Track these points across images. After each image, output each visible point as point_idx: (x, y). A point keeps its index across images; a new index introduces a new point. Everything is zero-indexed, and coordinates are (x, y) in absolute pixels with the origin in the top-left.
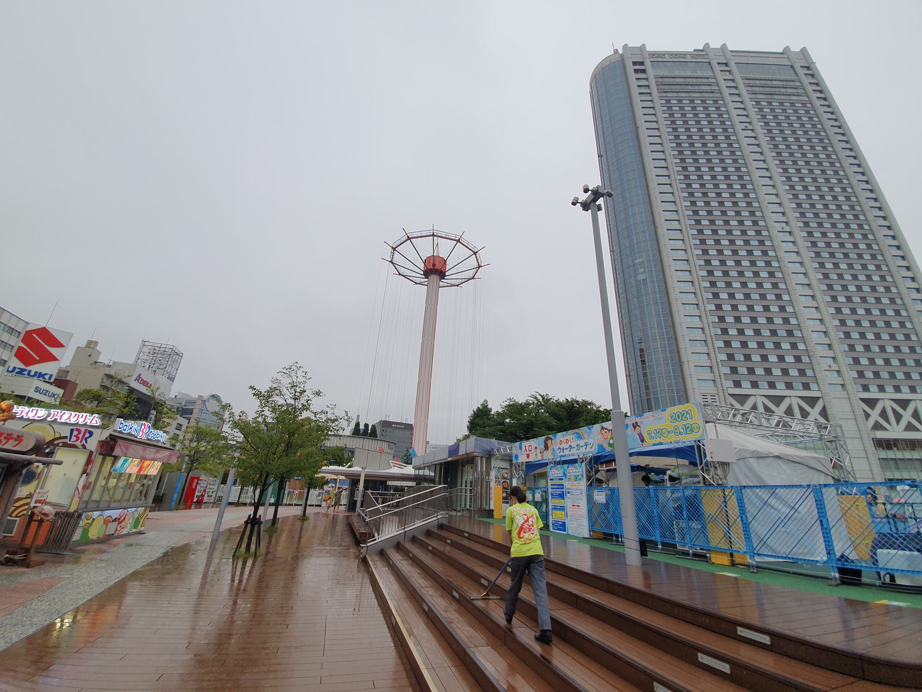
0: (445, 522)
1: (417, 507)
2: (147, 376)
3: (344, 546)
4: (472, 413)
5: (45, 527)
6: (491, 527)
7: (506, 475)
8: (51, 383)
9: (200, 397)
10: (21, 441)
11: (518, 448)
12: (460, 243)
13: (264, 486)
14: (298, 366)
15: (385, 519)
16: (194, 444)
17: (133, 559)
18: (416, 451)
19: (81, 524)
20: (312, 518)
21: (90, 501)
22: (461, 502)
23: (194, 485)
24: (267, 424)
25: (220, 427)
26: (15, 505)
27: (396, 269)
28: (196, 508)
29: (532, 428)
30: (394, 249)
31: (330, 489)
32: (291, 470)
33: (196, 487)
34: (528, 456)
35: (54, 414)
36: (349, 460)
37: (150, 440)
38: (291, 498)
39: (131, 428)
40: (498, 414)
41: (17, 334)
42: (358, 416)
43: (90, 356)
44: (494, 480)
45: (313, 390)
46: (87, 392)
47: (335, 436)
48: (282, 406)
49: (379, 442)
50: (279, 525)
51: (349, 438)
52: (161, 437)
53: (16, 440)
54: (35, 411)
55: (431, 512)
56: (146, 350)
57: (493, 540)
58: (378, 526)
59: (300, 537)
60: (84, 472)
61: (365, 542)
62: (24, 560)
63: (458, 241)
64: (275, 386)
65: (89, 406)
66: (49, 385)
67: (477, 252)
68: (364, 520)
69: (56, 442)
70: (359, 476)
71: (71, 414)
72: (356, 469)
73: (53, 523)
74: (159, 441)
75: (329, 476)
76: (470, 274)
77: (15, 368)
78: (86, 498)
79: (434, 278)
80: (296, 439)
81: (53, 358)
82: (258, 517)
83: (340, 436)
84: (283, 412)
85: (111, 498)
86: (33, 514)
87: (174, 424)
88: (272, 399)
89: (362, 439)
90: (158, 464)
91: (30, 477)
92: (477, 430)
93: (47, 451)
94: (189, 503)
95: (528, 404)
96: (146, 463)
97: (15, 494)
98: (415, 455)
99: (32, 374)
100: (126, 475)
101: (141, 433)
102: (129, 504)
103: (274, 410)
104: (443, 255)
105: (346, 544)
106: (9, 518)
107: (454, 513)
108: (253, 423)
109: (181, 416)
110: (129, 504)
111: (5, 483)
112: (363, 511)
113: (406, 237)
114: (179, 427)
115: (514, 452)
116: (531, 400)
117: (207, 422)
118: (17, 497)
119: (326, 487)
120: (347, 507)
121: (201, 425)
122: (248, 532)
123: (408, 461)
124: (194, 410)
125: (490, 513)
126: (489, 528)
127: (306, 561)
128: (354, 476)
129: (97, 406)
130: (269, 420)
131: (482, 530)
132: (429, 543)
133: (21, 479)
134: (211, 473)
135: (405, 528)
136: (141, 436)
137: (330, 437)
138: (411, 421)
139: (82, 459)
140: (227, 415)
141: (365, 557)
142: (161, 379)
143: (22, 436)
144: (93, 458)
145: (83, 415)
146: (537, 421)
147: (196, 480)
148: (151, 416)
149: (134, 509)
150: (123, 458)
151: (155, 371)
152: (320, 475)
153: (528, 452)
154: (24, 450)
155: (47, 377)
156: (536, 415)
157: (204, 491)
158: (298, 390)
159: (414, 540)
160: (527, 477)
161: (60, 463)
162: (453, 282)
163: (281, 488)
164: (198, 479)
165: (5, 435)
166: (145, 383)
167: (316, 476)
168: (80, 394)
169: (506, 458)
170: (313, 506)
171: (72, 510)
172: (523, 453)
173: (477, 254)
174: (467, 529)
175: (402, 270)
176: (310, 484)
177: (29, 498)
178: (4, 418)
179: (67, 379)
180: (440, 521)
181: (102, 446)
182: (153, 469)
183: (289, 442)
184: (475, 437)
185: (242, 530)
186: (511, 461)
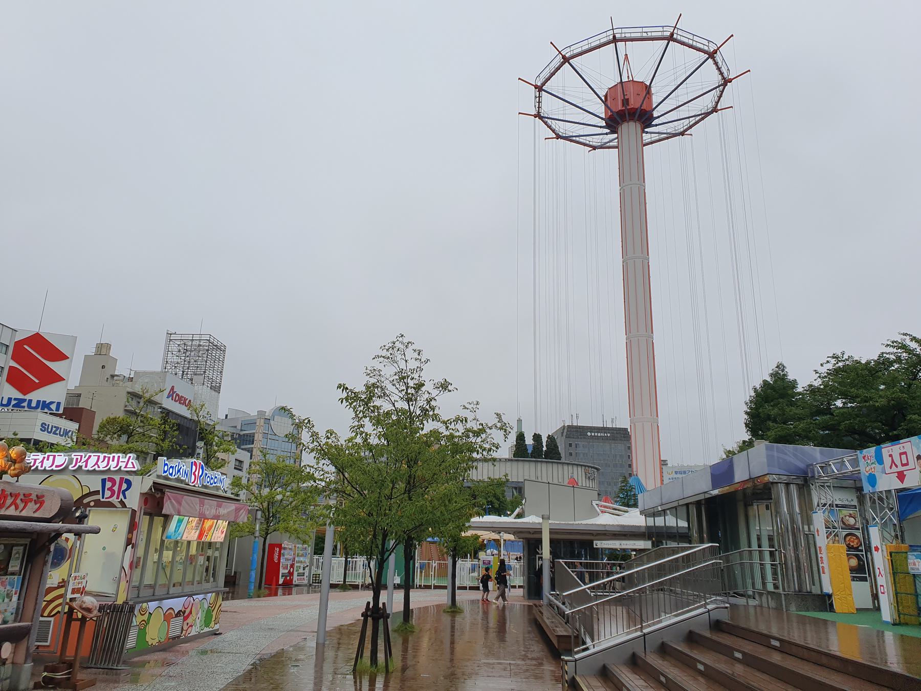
0: (725, 617)
1: (660, 588)
2: (183, 389)
3: (532, 659)
4: (753, 394)
5: (90, 627)
6: (831, 629)
7: (852, 521)
8: (60, 416)
9: (261, 413)
10: (42, 503)
11: (873, 460)
12: (676, 41)
13: (382, 553)
14: (405, 340)
15: (601, 612)
16: (266, 491)
17: (213, 673)
18: (643, 481)
19: (136, 621)
20: (467, 609)
21: (142, 587)
22: (753, 578)
23: (276, 557)
24: (370, 448)
25: (299, 458)
26: (45, 599)
27: (549, 127)
28: (284, 594)
29: (904, 416)
30: (539, 88)
31: (491, 558)
32: (422, 525)
33: (279, 559)
34: (901, 476)
35: (77, 459)
36: (516, 503)
37: (206, 487)
38: (427, 576)
39: (179, 471)
40: (812, 390)
41: (4, 348)
42: (519, 421)
43: (103, 367)
44: (823, 531)
45: (436, 381)
46: (112, 421)
47: (485, 460)
48: (388, 414)
49: (566, 467)
50: (414, 621)
51: (509, 464)
52: (222, 481)
53: (36, 503)
54: (51, 458)
55: (691, 598)
56: (174, 348)
57: (838, 654)
58: (589, 623)
59: (452, 643)
60: (129, 542)
61: (569, 652)
62: (68, 679)
63: (671, 38)
64: (373, 381)
65: (115, 443)
66: (58, 419)
67: (715, 52)
68: (562, 614)
69: (85, 501)
70: (539, 531)
71: (99, 456)
72: (532, 520)
73: (99, 621)
74: (218, 488)
75: (486, 535)
76: (707, 102)
77: (10, 400)
78: (135, 582)
79: (630, 129)
80: (420, 471)
81: (57, 378)
82: (381, 605)
83: (494, 460)
84: (393, 424)
85: (170, 581)
86: (71, 609)
87: (231, 459)
88: (372, 404)
89: (533, 465)
90: (223, 525)
91: (61, 556)
92: (769, 429)
93: (77, 514)
94: (274, 587)
95: (883, 363)
96: (208, 524)
97: (45, 583)
98: (642, 489)
99: (34, 404)
100: (182, 543)
101: (193, 477)
102: (196, 587)
103: (377, 422)
104: (643, 75)
105: (535, 655)
106: (41, 619)
107: (741, 601)
108: (348, 448)
109: (239, 447)
110: (196, 587)
111: (30, 565)
112: (556, 596)
113: (559, 59)
114: (239, 465)
115: (864, 469)
116: (891, 353)
117: (279, 452)
118: (48, 586)
119: (482, 555)
120: (526, 590)
121: (271, 459)
122: (369, 633)
123: (628, 500)
124: (256, 436)
125: (825, 602)
126: (827, 633)
127: (469, 683)
128: (529, 533)
129: (127, 442)
130: (373, 441)
131: (809, 635)
132: (698, 657)
133: (50, 558)
134: (297, 535)
135: (641, 629)
136: (194, 482)
137: (475, 464)
138: (623, 422)
139: (123, 523)
140: (305, 437)
141: (573, 679)
142: (198, 392)
143: (43, 496)
144: (137, 520)
145: (114, 457)
146: (914, 398)
147: (278, 549)
148: (198, 451)
149: (201, 597)
150: (176, 518)
151: (191, 380)
152: (469, 533)
153: (900, 468)
154: (49, 515)
155: (53, 407)
156: (910, 386)
157: (292, 566)
158: (411, 383)
159: (664, 650)
160: (905, 524)
161: (96, 531)
162: (670, 128)
163: (409, 557)
164: (280, 546)
165: (22, 497)
166: (181, 400)
167: (463, 534)
168: (102, 427)
169: (845, 483)
170: (464, 588)
171: (120, 601)
172: (888, 470)
173: (718, 57)
174: (774, 631)
175: (561, 128)
176: (455, 549)
177: (62, 587)
178: (16, 472)
179: (80, 406)
180: (715, 616)
181: (146, 502)
182: (218, 533)
183: (410, 476)
184: (767, 443)
185: (359, 628)
186: (860, 489)
